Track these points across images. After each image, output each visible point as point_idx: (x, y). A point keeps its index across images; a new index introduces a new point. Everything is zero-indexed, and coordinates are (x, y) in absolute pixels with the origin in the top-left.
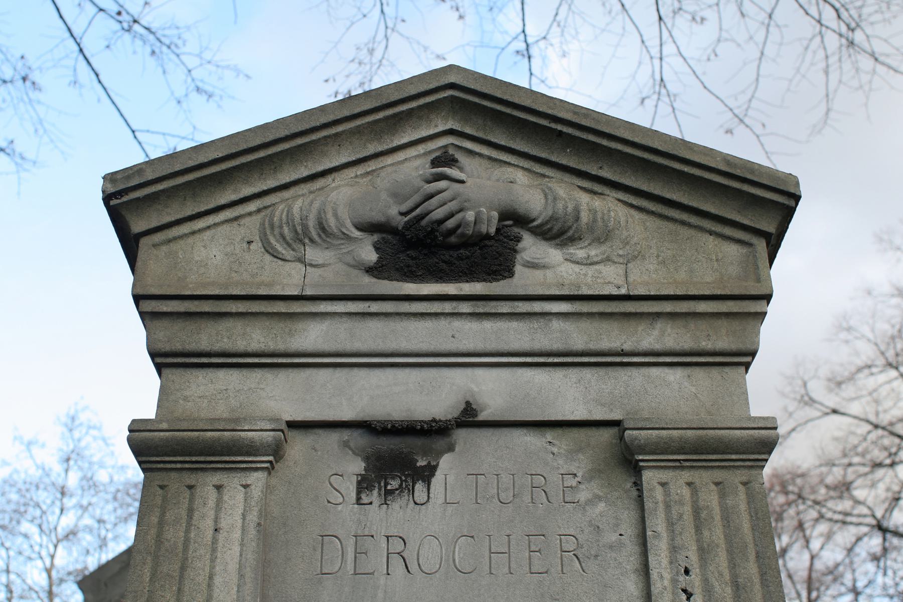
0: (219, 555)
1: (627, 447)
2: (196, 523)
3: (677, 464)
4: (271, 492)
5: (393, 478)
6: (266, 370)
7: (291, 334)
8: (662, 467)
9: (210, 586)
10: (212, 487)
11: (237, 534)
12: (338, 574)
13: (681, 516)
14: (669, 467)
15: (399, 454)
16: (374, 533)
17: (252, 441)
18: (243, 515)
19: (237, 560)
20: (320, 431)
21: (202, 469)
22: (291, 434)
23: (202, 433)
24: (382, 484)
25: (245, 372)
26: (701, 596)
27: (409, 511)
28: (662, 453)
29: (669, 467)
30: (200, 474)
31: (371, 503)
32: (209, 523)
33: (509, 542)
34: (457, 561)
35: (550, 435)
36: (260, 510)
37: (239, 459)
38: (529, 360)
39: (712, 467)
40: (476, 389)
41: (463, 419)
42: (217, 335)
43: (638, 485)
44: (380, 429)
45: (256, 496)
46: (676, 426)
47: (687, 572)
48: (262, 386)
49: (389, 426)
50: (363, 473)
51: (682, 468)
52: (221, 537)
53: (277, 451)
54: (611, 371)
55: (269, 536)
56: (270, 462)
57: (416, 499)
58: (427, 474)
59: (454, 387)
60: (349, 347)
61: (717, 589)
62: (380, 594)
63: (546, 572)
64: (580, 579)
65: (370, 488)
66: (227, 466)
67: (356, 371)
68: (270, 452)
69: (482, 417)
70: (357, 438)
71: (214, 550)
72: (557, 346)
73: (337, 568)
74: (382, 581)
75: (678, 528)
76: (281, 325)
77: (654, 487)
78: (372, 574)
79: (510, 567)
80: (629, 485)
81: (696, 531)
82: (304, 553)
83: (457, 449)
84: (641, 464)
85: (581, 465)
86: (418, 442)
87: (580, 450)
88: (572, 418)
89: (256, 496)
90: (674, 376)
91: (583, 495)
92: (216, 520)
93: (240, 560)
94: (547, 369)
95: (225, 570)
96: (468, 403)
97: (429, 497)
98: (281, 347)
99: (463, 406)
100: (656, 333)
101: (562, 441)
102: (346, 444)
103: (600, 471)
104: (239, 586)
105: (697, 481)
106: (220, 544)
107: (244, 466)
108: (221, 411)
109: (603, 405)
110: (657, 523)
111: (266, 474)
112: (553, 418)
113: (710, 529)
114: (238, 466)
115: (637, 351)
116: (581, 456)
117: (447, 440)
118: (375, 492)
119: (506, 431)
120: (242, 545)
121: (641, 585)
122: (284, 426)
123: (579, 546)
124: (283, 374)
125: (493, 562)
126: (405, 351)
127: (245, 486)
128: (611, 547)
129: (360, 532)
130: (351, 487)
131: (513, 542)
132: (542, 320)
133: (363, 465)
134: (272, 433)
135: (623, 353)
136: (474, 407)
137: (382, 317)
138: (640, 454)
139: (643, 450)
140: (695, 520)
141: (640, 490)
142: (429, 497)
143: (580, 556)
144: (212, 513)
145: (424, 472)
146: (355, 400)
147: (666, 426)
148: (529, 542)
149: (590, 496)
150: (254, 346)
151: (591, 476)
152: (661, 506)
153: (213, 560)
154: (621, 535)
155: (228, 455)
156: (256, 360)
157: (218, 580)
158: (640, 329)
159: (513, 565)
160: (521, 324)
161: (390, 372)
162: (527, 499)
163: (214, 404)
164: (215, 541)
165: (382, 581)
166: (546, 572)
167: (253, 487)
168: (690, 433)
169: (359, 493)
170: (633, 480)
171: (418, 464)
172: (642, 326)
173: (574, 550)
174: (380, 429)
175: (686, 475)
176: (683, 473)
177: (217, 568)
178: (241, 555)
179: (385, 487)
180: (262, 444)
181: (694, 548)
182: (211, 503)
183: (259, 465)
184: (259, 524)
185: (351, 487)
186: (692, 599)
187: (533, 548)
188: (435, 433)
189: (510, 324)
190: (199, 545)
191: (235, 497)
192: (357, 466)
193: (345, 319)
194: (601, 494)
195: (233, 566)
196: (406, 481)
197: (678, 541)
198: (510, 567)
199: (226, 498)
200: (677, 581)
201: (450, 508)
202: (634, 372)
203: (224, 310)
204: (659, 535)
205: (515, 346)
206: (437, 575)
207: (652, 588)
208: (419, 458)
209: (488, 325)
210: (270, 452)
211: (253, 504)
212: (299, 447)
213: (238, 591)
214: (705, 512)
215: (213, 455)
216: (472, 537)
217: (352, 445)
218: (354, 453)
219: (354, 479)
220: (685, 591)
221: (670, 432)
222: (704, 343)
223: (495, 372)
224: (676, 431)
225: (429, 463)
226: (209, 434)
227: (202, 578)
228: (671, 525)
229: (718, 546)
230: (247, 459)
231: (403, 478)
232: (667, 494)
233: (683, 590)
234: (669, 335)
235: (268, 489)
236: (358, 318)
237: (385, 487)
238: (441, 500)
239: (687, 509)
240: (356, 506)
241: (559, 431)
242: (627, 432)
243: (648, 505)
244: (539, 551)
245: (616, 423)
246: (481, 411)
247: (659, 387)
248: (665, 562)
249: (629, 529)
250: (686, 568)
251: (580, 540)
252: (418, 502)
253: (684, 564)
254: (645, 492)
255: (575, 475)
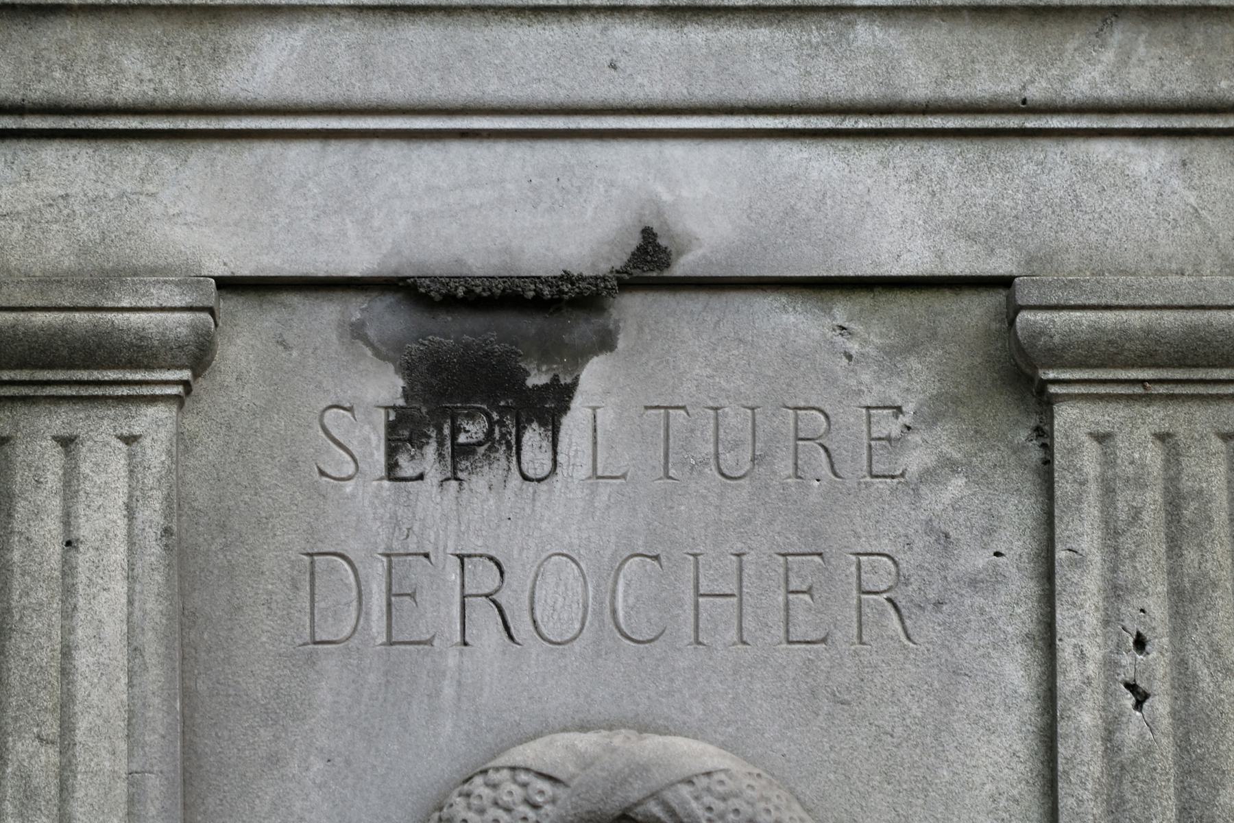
0: (81, 602)
1: (1020, 349)
2: (22, 528)
3: (1138, 390)
4: (187, 450)
5: (471, 417)
6: (158, 144)
7: (217, 59)
8: (1100, 397)
9: (66, 672)
10: (49, 443)
11: (118, 554)
12: (351, 644)
13: (1136, 514)
14: (1118, 398)
15: (484, 359)
16: (429, 548)
17: (141, 334)
18: (128, 507)
19: (121, 613)
20: (295, 299)
21: (25, 399)
22: (229, 305)
23: (22, 316)
24: (447, 431)
25: (107, 149)
26: (1167, 699)
27: (508, 493)
28: (1102, 365)
29: (1118, 398)
30: (21, 410)
31: (421, 477)
32: (49, 529)
33: (741, 570)
34: (621, 614)
35: (842, 309)
36: (167, 497)
37: (112, 375)
38: (796, 122)
39: (1219, 398)
40: (666, 197)
41: (637, 272)
42: (36, 59)
43: (1043, 434)
44: (438, 298)
45: (155, 463)
46: (1139, 301)
47: (1140, 643)
48: (150, 188)
49: (461, 292)
50: (401, 402)
51: (1148, 399)
52: (83, 559)
53: (200, 355)
54: (1000, 152)
55: (193, 555)
56: (186, 384)
57: (524, 467)
58: (550, 407)
59: (615, 192)
60: (359, 93)
61: (1206, 683)
62: (448, 690)
63: (824, 640)
64: (900, 657)
65: (417, 441)
66: (83, 392)
67: (376, 148)
68: (184, 360)
69: (680, 268)
70: (387, 318)
71: (68, 591)
72: (865, 91)
73: (347, 630)
74: (452, 660)
75: (1127, 543)
76: (193, 35)
77: (1081, 444)
78: (429, 642)
79: (741, 629)
80: (1023, 435)
81: (1170, 549)
82: (270, 593)
83: (621, 344)
84: (1053, 389)
85: (913, 385)
86: (530, 325)
87: (913, 347)
88: (896, 270)
89: (155, 463)
90: (1149, 161)
91: (915, 460)
92: (67, 519)
93: (130, 614)
94: (842, 144)
95: (98, 638)
96: (648, 234)
97: (555, 461)
98: (195, 92)
99: (635, 241)
100: (1109, 56)
101: (868, 327)
102: (357, 332)
103: (957, 401)
104: (131, 673)
105: (1181, 431)
106: (82, 578)
107: (124, 391)
108: (57, 251)
109: (972, 238)
110: (1082, 532)
111: (174, 408)
112: (851, 270)
113: (1200, 545)
114: (110, 391)
115: (1059, 103)
116: (914, 363)
117: (597, 321)
118: (431, 450)
119: (737, 300)
120: (131, 578)
121: (1036, 671)
122: (210, 295)
123: (901, 579)
124: (200, 157)
125: (703, 616)
126: (495, 104)
127: (130, 440)
128: (973, 583)
129: (397, 546)
130: (374, 438)
131: (749, 570)
132: (831, 24)
133: (400, 383)
134: (187, 316)
135: (1026, 108)
136: (662, 242)
137: (439, 16)
138: (1051, 367)
139: (1057, 358)
140: (1169, 523)
141: (1047, 448)
142: (555, 461)
143: (902, 603)
144: (56, 504)
145: (544, 400)
146: (376, 224)
147: (1115, 302)
148: (787, 570)
149: (930, 460)
150: (128, 91)
151: (933, 414)
152: (1093, 488)
153: (68, 613)
154: (997, 554)
155: (87, 368)
156: (134, 123)
157: (83, 660)
158: (1070, 46)
159: (749, 623)
160: (779, 34)
161: (457, 149)
162: (784, 467)
163: (38, 234)
164: (68, 569)
165: (452, 660)
166: (824, 640)
167: (147, 442)
168: (1169, 317)
169: (392, 452)
170: (1034, 421)
171: (532, 381)
172: (1074, 40)
173: (890, 589)
174: (438, 298)
175: (1157, 417)
176: (1150, 410)
177: (80, 633)
178: (130, 602)
179: (454, 437)
180: (164, 343)
181: (1162, 588)
182: (53, 480)
183: (158, 391)
184: (167, 531)
185: (374, 438)
186: (1146, 705)
187: (795, 584)
188: (566, 308)
189: (752, 33)
190: (34, 579)
191: (105, 467)
192: (385, 387)
193: (346, 21)
194: (957, 456)
195: (114, 630)
196: (501, 423)
197: (1126, 574)
198: (741, 629)
199: (85, 468)
200: (1117, 664)
201: (605, 490)
202: (1052, 151)
203: (55, 84)
204: (1083, 558)
205: (765, 90)
206: (576, 645)
207: (1060, 681)
208: (531, 366)
209: (698, 35)
210: (184, 360)
211: (150, 481)
212: (246, 337)
213: (130, 685)
214: (1193, 505)
215: (51, 366)
216: (656, 558)
217: (371, 333)
218: (377, 354)
219: (380, 418)
220: (1132, 687)
221: (1124, 315)
222: (1224, 84)
223: (714, 151)
224: (1137, 314)
225: (555, 379)
226: (40, 318)
227: (47, 656)
228: (1112, 533)
229: (1215, 585)
230: (130, 376)
231: (495, 416)
232: (1109, 461)
233: (1127, 686)
234: (1141, 62)
235: (182, 442)
236: (380, 17)
237: (454, 437)
238: (585, 471)
239: (1153, 497)
240: (386, 483)
241: (865, 300)
242: (1024, 316)
243: (1064, 487)
244: (809, 591)
245: (1004, 283)
246: (680, 253)
247: (1110, 192)
248: (1092, 620)
249: (1017, 543)
250: (1139, 634)
251: (903, 565)
252: (531, 474)
253: (1133, 627)
254: (1057, 456)
255: (899, 409)
